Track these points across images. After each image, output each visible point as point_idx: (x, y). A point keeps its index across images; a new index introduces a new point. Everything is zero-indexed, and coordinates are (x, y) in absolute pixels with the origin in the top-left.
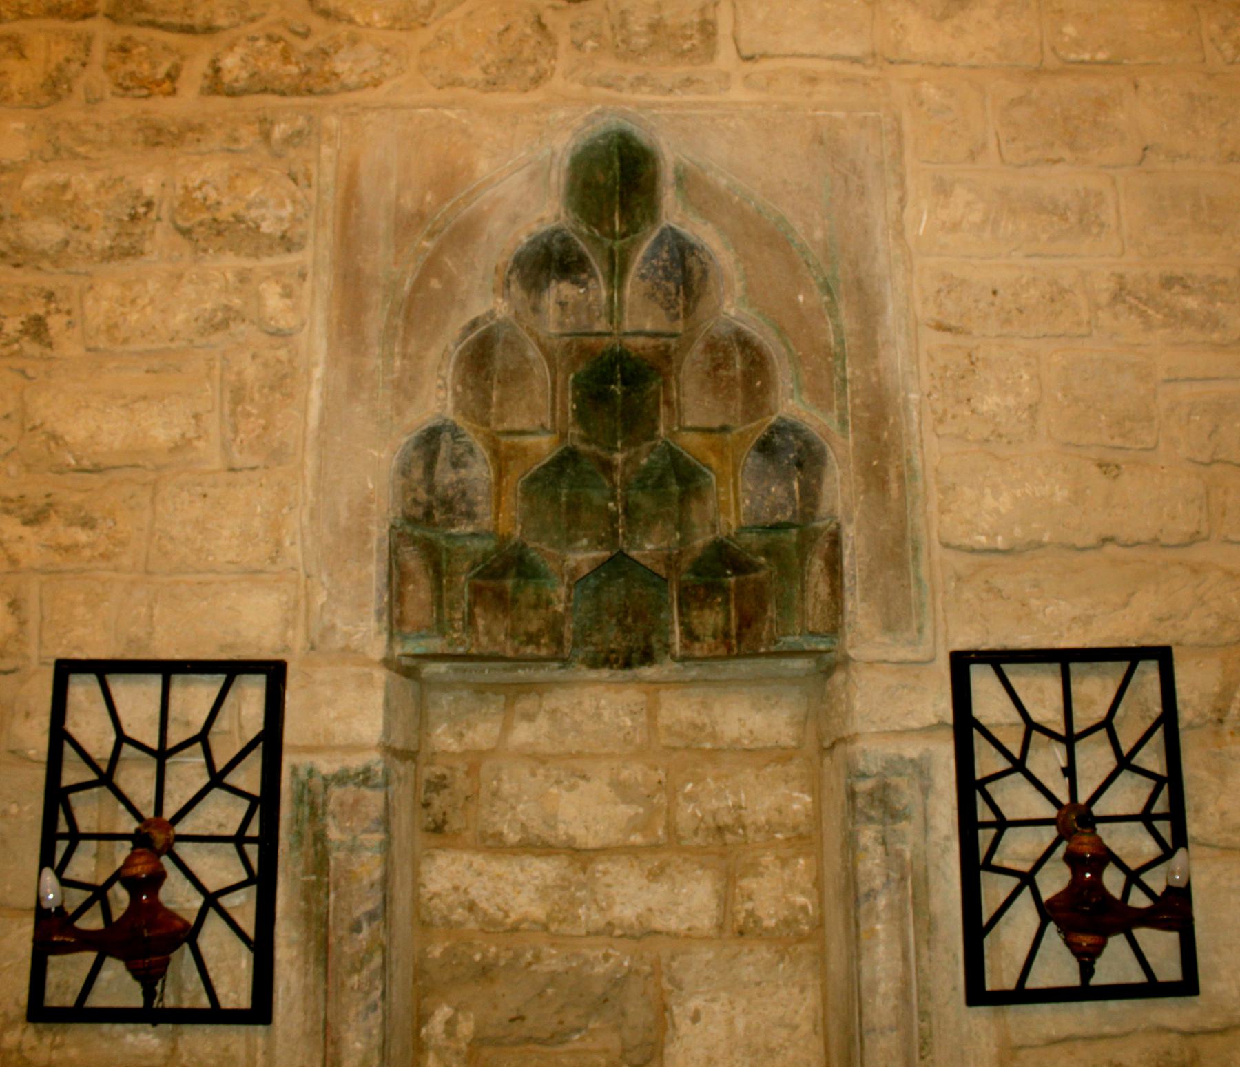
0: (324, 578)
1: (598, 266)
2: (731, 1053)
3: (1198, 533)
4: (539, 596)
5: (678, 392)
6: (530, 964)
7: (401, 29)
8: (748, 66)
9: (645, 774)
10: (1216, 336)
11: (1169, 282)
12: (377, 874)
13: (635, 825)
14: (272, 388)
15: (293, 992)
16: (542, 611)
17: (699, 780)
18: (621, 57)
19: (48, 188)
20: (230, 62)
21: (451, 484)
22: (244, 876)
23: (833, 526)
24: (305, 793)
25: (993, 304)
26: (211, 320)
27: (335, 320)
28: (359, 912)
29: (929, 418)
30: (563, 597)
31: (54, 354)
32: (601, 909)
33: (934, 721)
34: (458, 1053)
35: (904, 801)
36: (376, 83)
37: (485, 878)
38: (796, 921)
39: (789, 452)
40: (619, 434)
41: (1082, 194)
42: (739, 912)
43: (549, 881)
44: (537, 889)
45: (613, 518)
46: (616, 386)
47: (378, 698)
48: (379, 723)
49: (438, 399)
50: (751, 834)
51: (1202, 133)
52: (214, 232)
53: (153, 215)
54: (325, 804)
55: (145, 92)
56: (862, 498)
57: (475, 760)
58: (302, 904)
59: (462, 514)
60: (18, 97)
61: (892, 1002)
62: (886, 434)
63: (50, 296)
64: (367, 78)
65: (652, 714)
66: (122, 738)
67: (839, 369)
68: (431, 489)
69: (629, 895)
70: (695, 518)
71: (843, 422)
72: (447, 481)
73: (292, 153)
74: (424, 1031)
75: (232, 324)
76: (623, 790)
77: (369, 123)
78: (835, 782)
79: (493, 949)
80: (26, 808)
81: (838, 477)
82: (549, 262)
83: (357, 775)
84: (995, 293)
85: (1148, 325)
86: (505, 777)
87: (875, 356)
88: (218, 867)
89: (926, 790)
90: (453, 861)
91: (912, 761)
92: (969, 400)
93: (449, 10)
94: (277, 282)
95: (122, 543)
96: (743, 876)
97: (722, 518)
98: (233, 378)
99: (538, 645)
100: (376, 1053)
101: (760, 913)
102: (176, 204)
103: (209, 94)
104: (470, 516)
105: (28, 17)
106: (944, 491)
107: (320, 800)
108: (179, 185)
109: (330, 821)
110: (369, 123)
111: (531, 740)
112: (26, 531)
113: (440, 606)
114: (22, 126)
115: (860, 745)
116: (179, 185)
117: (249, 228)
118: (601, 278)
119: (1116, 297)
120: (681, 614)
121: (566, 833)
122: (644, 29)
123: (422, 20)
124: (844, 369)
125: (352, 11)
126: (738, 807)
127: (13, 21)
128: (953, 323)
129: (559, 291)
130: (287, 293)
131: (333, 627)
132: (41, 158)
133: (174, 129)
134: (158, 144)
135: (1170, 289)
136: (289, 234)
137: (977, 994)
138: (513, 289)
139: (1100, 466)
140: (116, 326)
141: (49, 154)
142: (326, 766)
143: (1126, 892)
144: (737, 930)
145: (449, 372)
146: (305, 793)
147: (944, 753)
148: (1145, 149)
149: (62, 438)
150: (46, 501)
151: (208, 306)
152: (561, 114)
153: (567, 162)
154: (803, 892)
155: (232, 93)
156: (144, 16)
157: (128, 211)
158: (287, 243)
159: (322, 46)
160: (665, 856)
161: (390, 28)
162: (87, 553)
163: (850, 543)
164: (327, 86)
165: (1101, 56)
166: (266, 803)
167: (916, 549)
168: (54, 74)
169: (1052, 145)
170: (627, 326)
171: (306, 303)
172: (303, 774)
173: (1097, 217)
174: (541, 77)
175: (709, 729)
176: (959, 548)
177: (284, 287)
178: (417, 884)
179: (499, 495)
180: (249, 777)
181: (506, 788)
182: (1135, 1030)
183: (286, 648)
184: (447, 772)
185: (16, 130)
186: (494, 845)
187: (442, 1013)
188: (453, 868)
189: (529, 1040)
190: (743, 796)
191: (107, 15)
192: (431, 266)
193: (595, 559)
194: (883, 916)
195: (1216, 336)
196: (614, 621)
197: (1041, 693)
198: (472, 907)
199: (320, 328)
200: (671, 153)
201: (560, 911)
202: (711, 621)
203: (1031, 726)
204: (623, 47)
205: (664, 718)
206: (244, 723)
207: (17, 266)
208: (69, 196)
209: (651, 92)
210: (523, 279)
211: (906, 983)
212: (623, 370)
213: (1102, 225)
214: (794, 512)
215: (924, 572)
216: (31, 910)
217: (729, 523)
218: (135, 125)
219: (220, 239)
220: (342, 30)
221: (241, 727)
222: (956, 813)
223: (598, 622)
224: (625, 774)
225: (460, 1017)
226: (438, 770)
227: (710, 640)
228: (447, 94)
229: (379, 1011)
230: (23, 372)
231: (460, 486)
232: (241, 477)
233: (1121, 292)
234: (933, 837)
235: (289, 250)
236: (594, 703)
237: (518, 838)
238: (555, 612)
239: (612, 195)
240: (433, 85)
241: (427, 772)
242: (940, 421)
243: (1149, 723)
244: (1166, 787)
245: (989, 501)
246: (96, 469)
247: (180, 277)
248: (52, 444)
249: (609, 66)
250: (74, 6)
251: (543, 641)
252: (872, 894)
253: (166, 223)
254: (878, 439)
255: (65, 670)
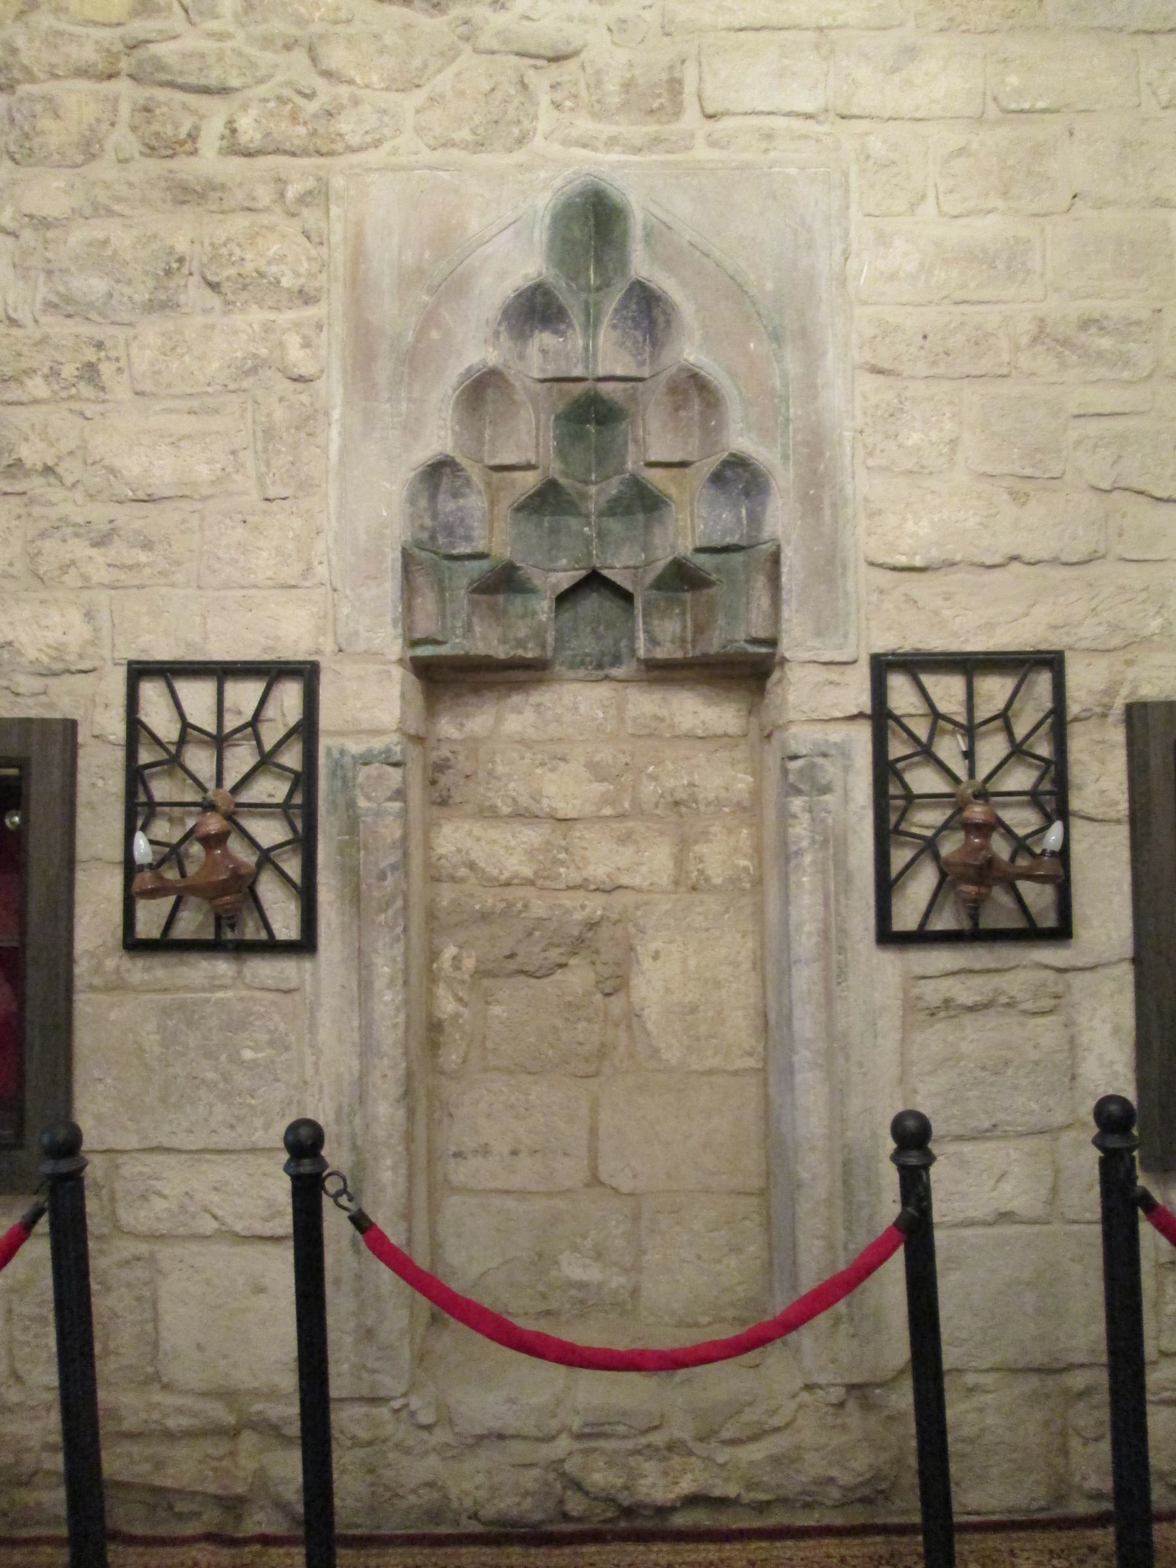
0: (348, 592)
1: (576, 317)
2: (685, 985)
3: (1095, 551)
4: (526, 608)
5: (644, 430)
6: (520, 912)
7: (397, 91)
8: (710, 125)
9: (615, 757)
10: (1126, 375)
11: (1085, 324)
12: (398, 834)
13: (606, 800)
14: (297, 428)
15: (333, 926)
16: (528, 621)
17: (660, 763)
18: (596, 116)
19: (91, 244)
20: (245, 123)
21: (452, 512)
22: (290, 836)
23: (774, 548)
24: (337, 767)
25: (922, 348)
26: (242, 366)
27: (349, 368)
28: (383, 864)
29: (861, 452)
30: (546, 609)
31: (107, 397)
32: (578, 868)
33: (855, 711)
34: (463, 982)
35: (828, 777)
36: (377, 144)
37: (484, 843)
38: (740, 880)
39: (739, 478)
40: (594, 468)
41: (1012, 243)
42: (692, 872)
43: (536, 846)
44: (526, 852)
45: (588, 541)
46: (591, 415)
47: (396, 691)
48: (397, 713)
49: (439, 437)
50: (702, 808)
51: (1130, 179)
52: (239, 286)
53: (185, 270)
54: (354, 778)
55: (170, 152)
56: (799, 523)
57: (473, 744)
58: (338, 858)
59: (460, 538)
60: (56, 157)
61: (814, 939)
62: (822, 467)
63: (100, 345)
64: (368, 139)
65: (621, 710)
66: (186, 725)
67: (783, 410)
68: (435, 516)
69: (601, 857)
70: (657, 541)
71: (785, 457)
72: (448, 510)
73: (305, 212)
74: (435, 965)
75: (260, 371)
76: (597, 771)
77: (373, 183)
78: (772, 760)
79: (490, 900)
80: (110, 782)
81: (780, 505)
82: (535, 310)
83: (380, 753)
84: (925, 337)
85: (1064, 365)
86: (498, 760)
87: (815, 398)
88: (269, 832)
89: (847, 769)
90: (456, 830)
91: (835, 744)
92: (896, 436)
93: (440, 71)
94: (298, 333)
95: (178, 564)
96: (696, 842)
97: (680, 541)
98: (263, 419)
99: (525, 648)
100: (400, 975)
101: (709, 872)
102: (205, 260)
103: (228, 153)
104: (468, 539)
105: (57, 77)
106: (871, 515)
107: (350, 774)
108: (207, 242)
109: (358, 792)
110: (373, 183)
111: (520, 729)
112: (93, 552)
113: (444, 616)
114: (62, 185)
115: (794, 729)
116: (207, 242)
117: (270, 283)
118: (578, 328)
119: (1035, 340)
120: (645, 623)
121: (549, 806)
122: (617, 88)
123: (416, 81)
124: (788, 409)
125: (352, 73)
126: (692, 785)
127: (44, 81)
128: (886, 366)
129: (541, 340)
130: (306, 345)
131: (356, 633)
132: (82, 216)
133: (198, 188)
134: (184, 202)
135: (1086, 331)
136: (306, 289)
137: (887, 936)
138: (502, 338)
139: (1011, 494)
140: (159, 372)
141: (88, 211)
142: (355, 747)
143: (1013, 859)
144: (686, 882)
145: (448, 413)
146: (337, 767)
147: (862, 734)
148: (1075, 196)
149: (119, 472)
150: (109, 526)
151: (239, 354)
152: (543, 174)
153: (547, 220)
154: (745, 856)
155: (248, 154)
156: (163, 77)
157: (163, 265)
158: (305, 297)
159: (327, 107)
160: (630, 824)
161: (388, 89)
162: (147, 571)
163: (788, 562)
164: (334, 147)
165: (1040, 105)
166: (305, 780)
167: (844, 567)
168: (87, 133)
169: (987, 195)
170: (601, 372)
171: (323, 352)
172: (336, 754)
173: (1024, 264)
174: (524, 138)
175: (668, 721)
176: (881, 566)
177: (304, 337)
178: (428, 846)
179: (492, 521)
180: (292, 758)
181: (500, 769)
182: (1017, 966)
183: (318, 652)
184: (449, 755)
185: (57, 188)
186: (488, 813)
187: (450, 951)
188: (457, 835)
189: (522, 972)
190: (696, 777)
191: (130, 76)
192: (430, 319)
193: (574, 577)
194: (809, 870)
195: (1126, 375)
196: (588, 630)
197: (948, 691)
198: (472, 866)
199: (336, 373)
200: (638, 202)
201: (544, 870)
202: (671, 629)
203: (936, 716)
204: (597, 106)
205: (631, 711)
206: (285, 711)
207: (69, 316)
208: (109, 252)
209: (624, 152)
210: (511, 328)
211: (825, 921)
212: (596, 413)
213: (1028, 272)
214: (742, 535)
215: (850, 587)
216: (120, 863)
217: (685, 546)
218: (163, 184)
219: (245, 293)
220: (344, 90)
221: (284, 715)
222: (871, 788)
223: (576, 630)
224: (598, 757)
225: (464, 954)
226: (444, 752)
227: (668, 645)
228: (438, 156)
229: (402, 942)
230: (82, 414)
231: (460, 514)
232: (274, 506)
233: (1041, 334)
234: (852, 807)
235: (306, 303)
236: (572, 698)
237: (510, 810)
238: (540, 621)
239: (588, 251)
240: (429, 146)
241: (434, 756)
242: (870, 454)
243: (1041, 715)
244: (1053, 768)
245: (910, 526)
246: (150, 500)
247: (213, 327)
248: (111, 477)
249: (584, 125)
250: (100, 67)
251: (530, 646)
252: (799, 853)
253: (196, 278)
254: (814, 471)
255: (139, 672)
